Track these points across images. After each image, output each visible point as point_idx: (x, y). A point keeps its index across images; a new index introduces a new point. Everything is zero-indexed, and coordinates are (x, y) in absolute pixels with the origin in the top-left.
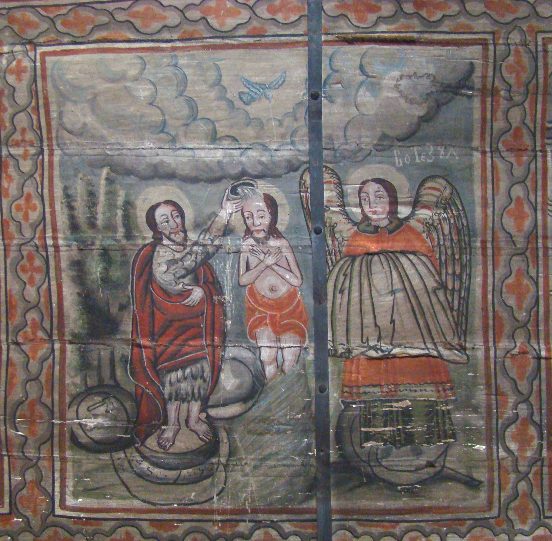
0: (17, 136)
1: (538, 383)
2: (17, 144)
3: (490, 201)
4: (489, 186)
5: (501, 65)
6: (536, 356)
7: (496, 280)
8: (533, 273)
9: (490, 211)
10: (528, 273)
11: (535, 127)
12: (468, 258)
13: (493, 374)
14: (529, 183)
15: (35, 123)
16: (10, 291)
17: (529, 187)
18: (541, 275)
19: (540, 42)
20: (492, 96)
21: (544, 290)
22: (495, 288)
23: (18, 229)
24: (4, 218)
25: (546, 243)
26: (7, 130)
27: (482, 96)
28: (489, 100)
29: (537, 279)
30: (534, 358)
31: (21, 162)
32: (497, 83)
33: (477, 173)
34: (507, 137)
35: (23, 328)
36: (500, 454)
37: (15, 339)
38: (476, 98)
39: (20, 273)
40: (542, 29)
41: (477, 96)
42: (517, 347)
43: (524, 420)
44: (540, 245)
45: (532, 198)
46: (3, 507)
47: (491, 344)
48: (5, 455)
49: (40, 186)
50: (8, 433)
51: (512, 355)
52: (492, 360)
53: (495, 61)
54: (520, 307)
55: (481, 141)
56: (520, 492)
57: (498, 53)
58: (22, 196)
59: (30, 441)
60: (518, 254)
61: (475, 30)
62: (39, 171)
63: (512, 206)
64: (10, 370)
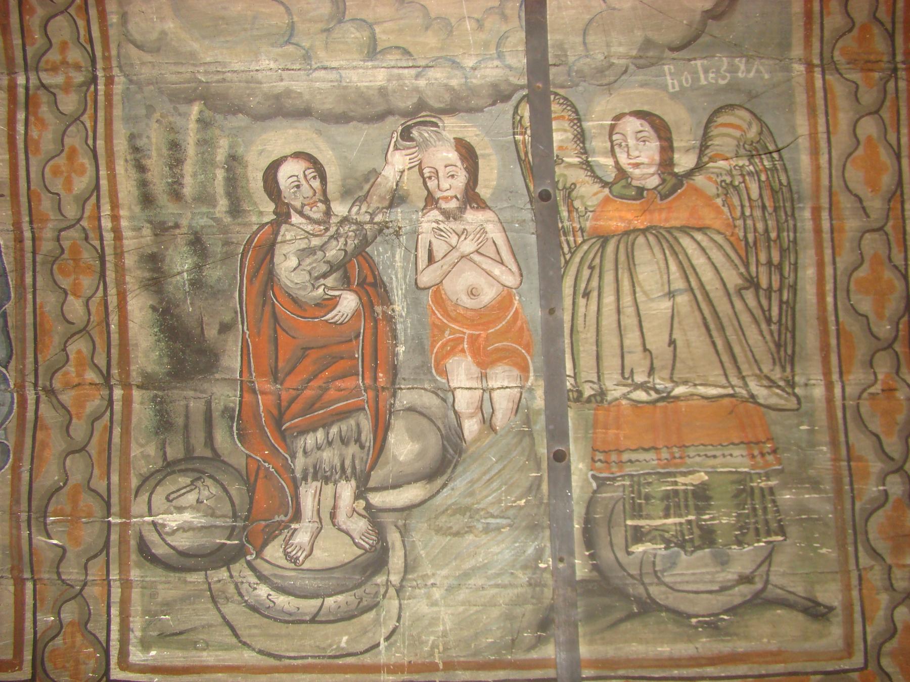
0: (54, 56)
2: (54, 69)
3: (823, 144)
4: (821, 120)
7: (839, 273)
9: (824, 160)
12: (791, 238)
14: (886, 114)
15: (82, 32)
16: (41, 307)
17: (887, 122)
22: (838, 286)
23: (57, 207)
24: (32, 188)
26: (37, 46)
31: (61, 96)
35: (63, 366)
36: (861, 561)
37: (48, 384)
39: (59, 277)
42: (879, 382)
45: (892, 137)
46: (20, 669)
47: (835, 377)
48: (28, 579)
49: (90, 134)
50: (34, 541)
52: (838, 403)
54: (880, 316)
56: (899, 626)
58: (62, 151)
59: (69, 555)
62: (90, 111)
63: (860, 151)
64: (40, 435)
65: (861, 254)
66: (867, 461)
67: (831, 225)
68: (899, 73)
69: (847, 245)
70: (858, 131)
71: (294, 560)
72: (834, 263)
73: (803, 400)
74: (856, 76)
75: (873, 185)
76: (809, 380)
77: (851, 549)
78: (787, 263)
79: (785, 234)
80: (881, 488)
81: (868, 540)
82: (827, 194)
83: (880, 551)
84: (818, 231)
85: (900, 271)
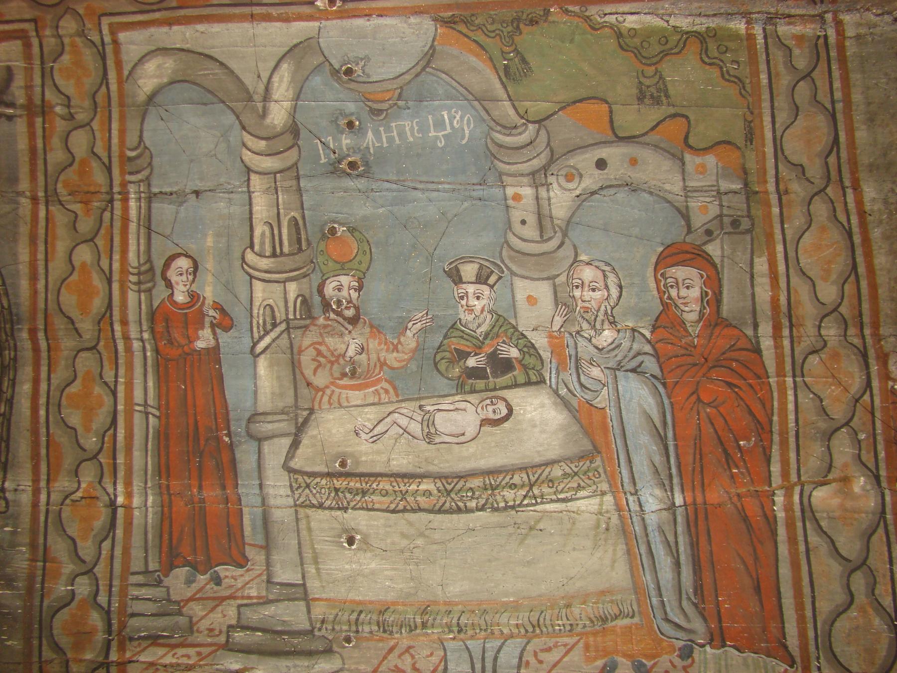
1: (110, 545)
3: (41, 270)
4: (41, 248)
5: (52, 68)
6: (108, 503)
7: (52, 388)
8: (109, 376)
10: (101, 377)
11: (110, 157)
12: (12, 356)
13: (42, 530)
14: (100, 242)
17: (101, 248)
18: (121, 380)
19: (106, 31)
20: (43, 114)
21: (126, 405)
22: (51, 401)
25: (128, 331)
27: (28, 115)
28: (39, 120)
29: (116, 386)
30: (106, 506)
32: (48, 95)
33: (24, 230)
34: (71, 174)
36: (44, 653)
38: (19, 120)
40: (109, 11)
41: (20, 116)
42: (81, 490)
43: (83, 600)
44: (118, 334)
45: (105, 264)
47: (43, 484)
51: (73, 501)
52: (43, 508)
53: (42, 63)
54: (88, 429)
55: (31, 181)
57: (46, 50)
60: (88, 349)
61: (8, 18)
63: (75, 277)
65: (75, 371)
66: (60, 562)
67: (49, 345)
68: (115, 203)
69: (63, 362)
70: (74, 258)
71: (497, 397)
72: (49, 379)
73: (11, 504)
74: (77, 207)
75: (84, 308)
76: (19, 485)
77: (35, 642)
78: (6, 379)
79: (7, 352)
80: (69, 588)
81: (52, 635)
82: (43, 316)
83: (62, 645)
84: (36, 349)
85: (109, 387)
